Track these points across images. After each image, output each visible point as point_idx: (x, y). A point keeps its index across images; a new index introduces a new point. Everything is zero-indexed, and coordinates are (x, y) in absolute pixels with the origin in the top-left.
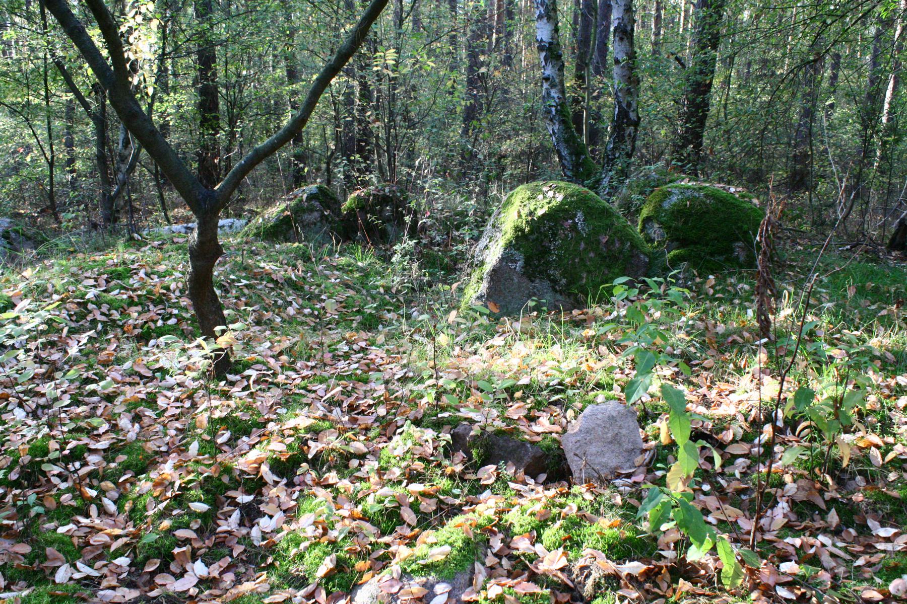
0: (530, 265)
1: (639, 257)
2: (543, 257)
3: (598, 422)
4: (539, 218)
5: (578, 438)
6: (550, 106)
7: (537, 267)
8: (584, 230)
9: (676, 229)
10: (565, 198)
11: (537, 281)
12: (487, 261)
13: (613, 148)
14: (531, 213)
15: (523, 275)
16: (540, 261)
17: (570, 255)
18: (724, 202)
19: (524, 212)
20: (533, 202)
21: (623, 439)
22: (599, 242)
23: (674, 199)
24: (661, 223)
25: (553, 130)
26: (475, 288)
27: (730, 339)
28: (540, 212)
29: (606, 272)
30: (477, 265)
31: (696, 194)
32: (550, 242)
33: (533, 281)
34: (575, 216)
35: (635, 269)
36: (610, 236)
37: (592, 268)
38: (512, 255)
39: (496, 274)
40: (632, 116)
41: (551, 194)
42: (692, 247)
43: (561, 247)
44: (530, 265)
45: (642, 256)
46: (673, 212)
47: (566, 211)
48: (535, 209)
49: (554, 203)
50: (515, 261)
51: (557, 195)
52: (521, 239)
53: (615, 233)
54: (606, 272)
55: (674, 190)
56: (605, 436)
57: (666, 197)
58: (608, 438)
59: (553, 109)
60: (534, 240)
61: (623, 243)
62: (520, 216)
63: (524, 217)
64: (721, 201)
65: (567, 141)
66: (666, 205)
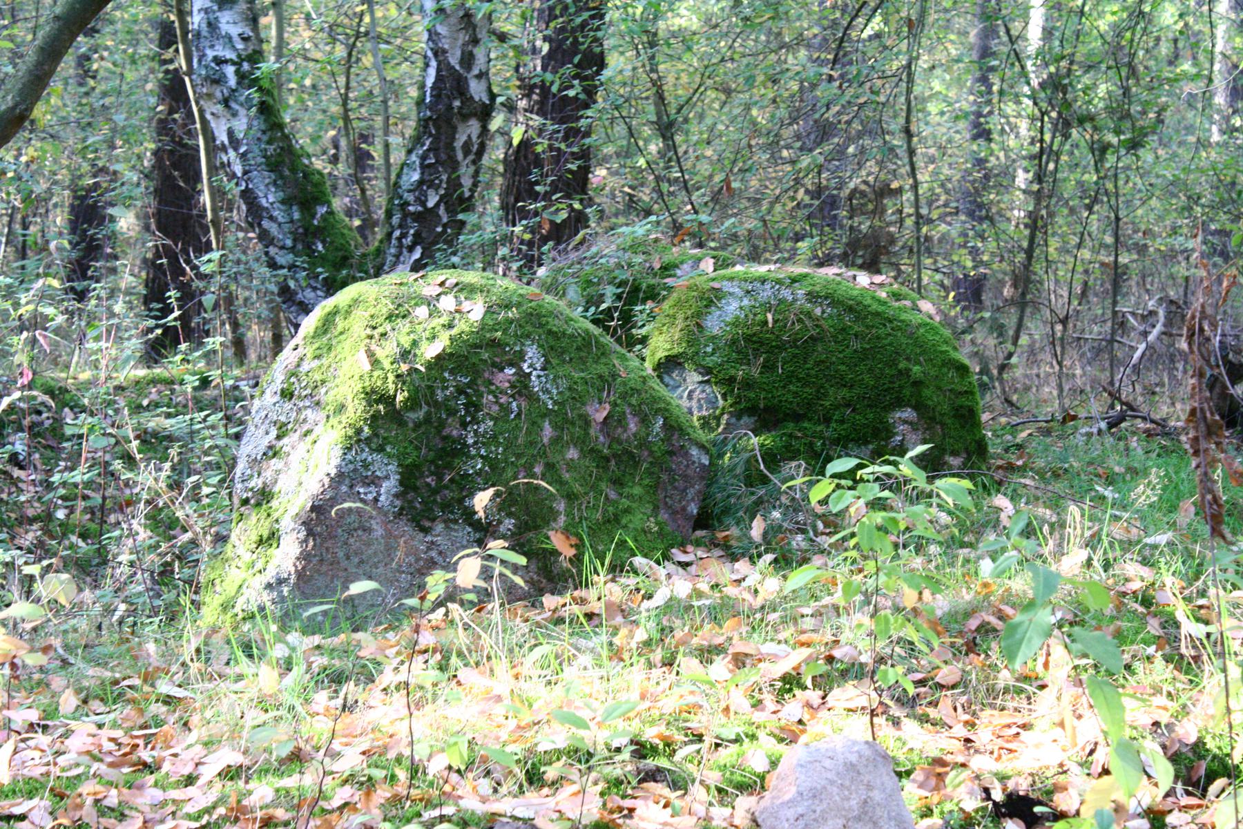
0: (415, 489)
1: (686, 454)
2: (449, 467)
3: (829, 776)
4: (429, 366)
5: (800, 810)
6: (219, 61)
7: (435, 492)
8: (547, 391)
9: (748, 384)
10: (489, 310)
11: (439, 527)
12: (284, 485)
13: (421, 182)
14: (405, 355)
15: (399, 515)
16: (440, 478)
17: (519, 456)
18: (854, 308)
19: (386, 352)
20: (403, 326)
21: (879, 812)
22: (586, 421)
23: (732, 308)
24: (707, 371)
25: (230, 133)
26: (250, 569)
27: (973, 624)
28: (430, 351)
29: (613, 495)
30: (246, 502)
31: (786, 294)
32: (464, 425)
33: (426, 531)
34: (521, 356)
35: (680, 484)
36: (615, 405)
37: (577, 488)
38: (366, 465)
39: (318, 519)
40: (477, 90)
41: (447, 303)
42: (790, 427)
43: (494, 437)
44: (415, 489)
45: (694, 452)
46: (734, 342)
47: (493, 343)
48: (415, 343)
49: (461, 326)
50: (374, 481)
51: (466, 306)
52: (384, 420)
53: (624, 396)
54: (613, 495)
55: (727, 286)
56: (846, 805)
57: (710, 303)
58: (851, 809)
59: (230, 70)
60: (417, 425)
61: (645, 421)
62: (375, 363)
63: (386, 364)
64: (851, 309)
65: (273, 165)
66: (714, 324)
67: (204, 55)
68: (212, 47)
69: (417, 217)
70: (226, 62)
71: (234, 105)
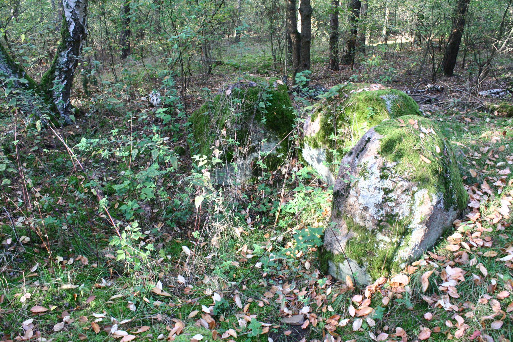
69: (65, 72)
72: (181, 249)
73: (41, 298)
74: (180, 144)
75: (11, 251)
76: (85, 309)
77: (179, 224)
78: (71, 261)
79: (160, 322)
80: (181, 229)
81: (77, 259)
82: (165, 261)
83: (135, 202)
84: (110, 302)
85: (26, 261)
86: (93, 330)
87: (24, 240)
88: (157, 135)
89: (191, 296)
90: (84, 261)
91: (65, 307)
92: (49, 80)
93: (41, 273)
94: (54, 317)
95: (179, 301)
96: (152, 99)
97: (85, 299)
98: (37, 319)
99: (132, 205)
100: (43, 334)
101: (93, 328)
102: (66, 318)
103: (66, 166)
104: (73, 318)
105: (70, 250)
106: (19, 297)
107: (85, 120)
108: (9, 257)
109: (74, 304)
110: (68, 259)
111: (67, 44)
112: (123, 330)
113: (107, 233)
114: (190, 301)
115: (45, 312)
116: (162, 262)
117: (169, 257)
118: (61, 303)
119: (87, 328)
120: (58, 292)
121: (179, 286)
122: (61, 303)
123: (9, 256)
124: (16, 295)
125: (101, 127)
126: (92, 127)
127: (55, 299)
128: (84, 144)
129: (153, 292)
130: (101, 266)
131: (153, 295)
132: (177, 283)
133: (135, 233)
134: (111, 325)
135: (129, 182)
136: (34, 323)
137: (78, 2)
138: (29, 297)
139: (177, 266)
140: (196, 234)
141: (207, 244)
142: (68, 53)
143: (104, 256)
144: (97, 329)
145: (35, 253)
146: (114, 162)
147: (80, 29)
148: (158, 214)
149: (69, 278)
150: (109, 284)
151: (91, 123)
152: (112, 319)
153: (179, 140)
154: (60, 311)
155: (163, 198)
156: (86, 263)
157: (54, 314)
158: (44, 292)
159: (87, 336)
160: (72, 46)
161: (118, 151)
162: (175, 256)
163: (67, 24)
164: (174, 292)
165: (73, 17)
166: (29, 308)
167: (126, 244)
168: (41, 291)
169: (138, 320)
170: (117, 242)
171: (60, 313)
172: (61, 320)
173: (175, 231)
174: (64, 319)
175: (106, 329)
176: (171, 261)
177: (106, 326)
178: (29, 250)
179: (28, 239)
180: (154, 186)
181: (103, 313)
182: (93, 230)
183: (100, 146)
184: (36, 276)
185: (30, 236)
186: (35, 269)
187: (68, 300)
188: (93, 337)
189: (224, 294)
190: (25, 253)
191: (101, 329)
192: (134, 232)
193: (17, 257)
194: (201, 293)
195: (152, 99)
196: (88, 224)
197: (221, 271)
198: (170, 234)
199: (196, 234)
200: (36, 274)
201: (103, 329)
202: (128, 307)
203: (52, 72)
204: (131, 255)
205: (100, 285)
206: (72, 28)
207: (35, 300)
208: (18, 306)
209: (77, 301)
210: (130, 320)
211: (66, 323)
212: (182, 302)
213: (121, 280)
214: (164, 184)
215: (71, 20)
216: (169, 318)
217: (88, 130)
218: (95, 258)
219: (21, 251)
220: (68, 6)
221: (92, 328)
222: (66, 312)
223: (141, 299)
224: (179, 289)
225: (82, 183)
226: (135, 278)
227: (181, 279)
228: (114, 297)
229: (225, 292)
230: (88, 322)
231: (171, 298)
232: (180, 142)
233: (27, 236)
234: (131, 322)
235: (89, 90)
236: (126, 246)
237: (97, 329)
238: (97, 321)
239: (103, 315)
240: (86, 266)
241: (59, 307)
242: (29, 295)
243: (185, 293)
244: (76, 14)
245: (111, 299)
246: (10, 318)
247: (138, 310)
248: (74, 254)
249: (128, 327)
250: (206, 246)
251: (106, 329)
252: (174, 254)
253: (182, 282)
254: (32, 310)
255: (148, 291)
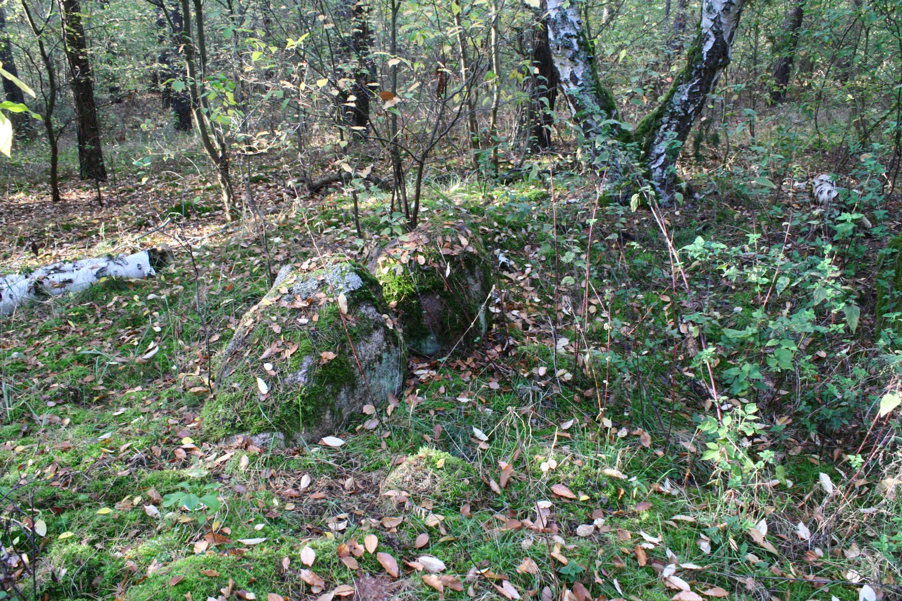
6: (568, 36)
59: (574, 41)
67: (559, 33)
68: (563, 28)
69: (681, 119)
70: (572, 36)
71: (577, 60)
72: (817, 478)
73: (570, 475)
74: (857, 283)
75: (541, 387)
76: (631, 520)
77: (821, 429)
78: (623, 433)
79: (747, 592)
80: (823, 442)
81: (634, 433)
82: (780, 488)
83: (756, 369)
84: (671, 523)
85: (557, 409)
86: (635, 559)
87: (562, 375)
88: (828, 261)
89: (816, 569)
90: (645, 440)
91: (601, 503)
92: (650, 129)
93: (576, 436)
94: (581, 512)
95: (792, 570)
96: (818, 189)
97: (634, 503)
98: (557, 505)
99: (749, 372)
100: (559, 532)
101: (637, 555)
102: (599, 522)
103: (650, 274)
104: (609, 526)
105: (626, 414)
106: (539, 461)
107: (692, 204)
108: (536, 395)
109: (614, 504)
110: (619, 428)
111: (693, 73)
112: (683, 578)
113: (688, 405)
114: (811, 577)
115: (571, 499)
116: (774, 487)
117: (790, 483)
118: (596, 495)
119: (626, 551)
120: (596, 476)
121: (797, 543)
122: (596, 495)
123: (538, 394)
124: (536, 456)
125: (719, 221)
126: (702, 219)
127: (590, 485)
128: (699, 248)
129: (748, 536)
130: (670, 458)
131: (745, 538)
132: (796, 536)
133: (747, 423)
134: (666, 562)
135: (755, 330)
136: (551, 509)
137: (730, 3)
138: (553, 468)
139: (800, 505)
140: (856, 460)
141: (868, 485)
142: (692, 89)
143: (677, 443)
144: (642, 561)
145: (574, 402)
146: (727, 287)
147: (721, 52)
148: (787, 399)
149: (618, 459)
150: (675, 492)
151: (701, 211)
152: (669, 553)
153: (856, 276)
154: (592, 506)
155: (807, 375)
156: (647, 444)
157: (583, 507)
158: (576, 468)
159: (625, 565)
160: (700, 76)
161: (754, 273)
162: (801, 485)
163: (702, 39)
164: (785, 549)
165: (714, 29)
166: (550, 483)
167: (727, 436)
168: (572, 465)
169: (711, 572)
170: (713, 428)
171: (591, 509)
172: (590, 522)
173: (810, 440)
174: (596, 522)
175: (655, 565)
176: (793, 492)
177: (656, 560)
178: (566, 394)
179: (568, 376)
180: (794, 348)
181: (657, 537)
182: (667, 393)
183: (724, 258)
184: (567, 438)
185: (573, 372)
186: (568, 425)
187: (608, 494)
188: (633, 569)
189: (885, 593)
190: (559, 396)
191: (648, 562)
192: (746, 421)
193: (548, 399)
194: (835, 572)
195: (818, 189)
196: (661, 380)
197: (890, 548)
198: (800, 442)
199: (856, 460)
200: (568, 435)
201: (651, 564)
202: (698, 543)
203: (658, 116)
204: (729, 457)
205: (661, 488)
206: (708, 46)
207: (561, 474)
208: (537, 475)
209: (621, 502)
210: (699, 568)
211: (597, 528)
212: (797, 574)
213: (696, 493)
214: (811, 349)
215: (710, 33)
216: (767, 594)
217: (694, 221)
218: (663, 441)
219: (555, 392)
220: (710, 9)
221: (634, 555)
222: (600, 511)
223: (725, 539)
224: (795, 547)
225: (665, 308)
226: (724, 498)
227: (803, 531)
228: (678, 517)
229: (888, 590)
230: (630, 543)
231: (777, 558)
232: (858, 280)
233: (569, 371)
234: (700, 571)
235: (701, 152)
236: (726, 440)
237: (642, 561)
238: (645, 545)
239: (656, 540)
240: (644, 449)
241: (593, 500)
242: (553, 464)
243: (806, 559)
244: (720, 23)
245: (674, 518)
246: (521, 487)
247: (714, 556)
248: (630, 423)
249: (695, 579)
250: (866, 489)
251: (655, 565)
252: (799, 482)
253: (804, 537)
254: (553, 488)
255: (741, 530)
